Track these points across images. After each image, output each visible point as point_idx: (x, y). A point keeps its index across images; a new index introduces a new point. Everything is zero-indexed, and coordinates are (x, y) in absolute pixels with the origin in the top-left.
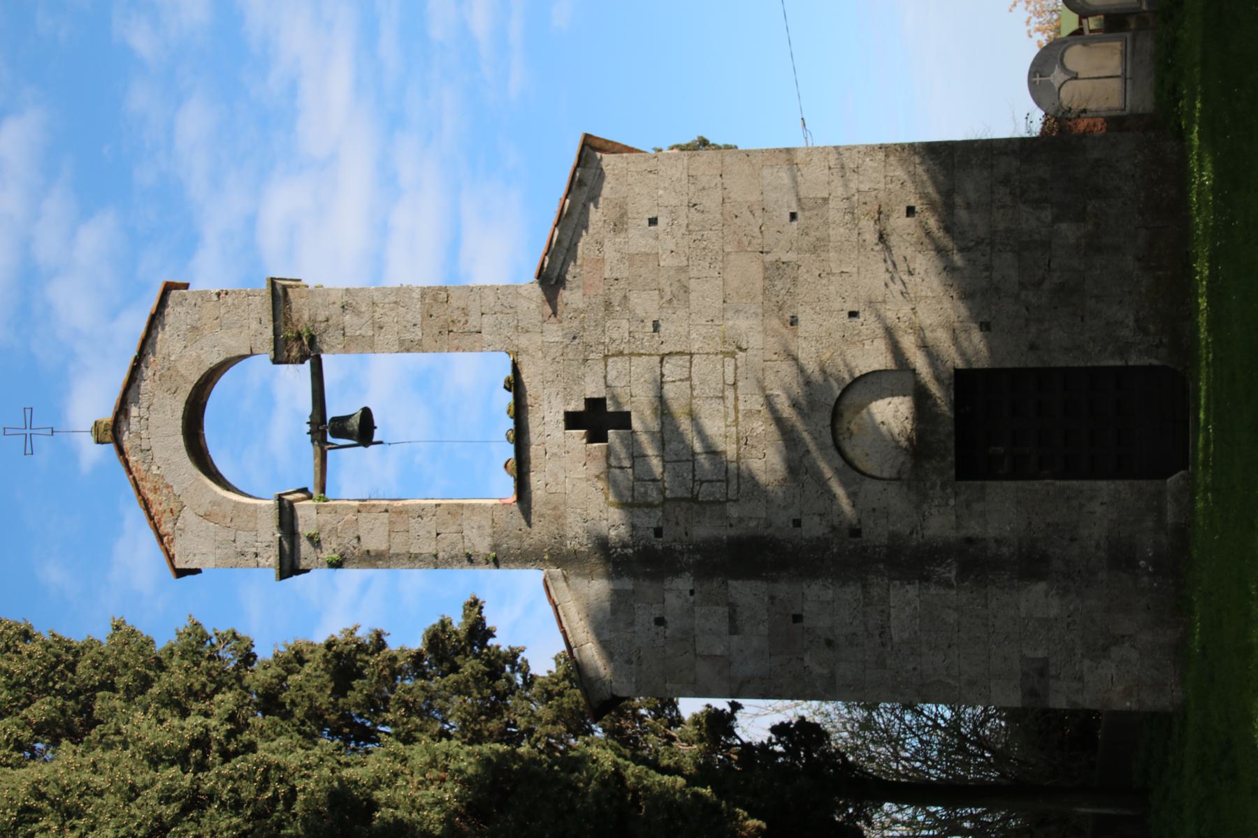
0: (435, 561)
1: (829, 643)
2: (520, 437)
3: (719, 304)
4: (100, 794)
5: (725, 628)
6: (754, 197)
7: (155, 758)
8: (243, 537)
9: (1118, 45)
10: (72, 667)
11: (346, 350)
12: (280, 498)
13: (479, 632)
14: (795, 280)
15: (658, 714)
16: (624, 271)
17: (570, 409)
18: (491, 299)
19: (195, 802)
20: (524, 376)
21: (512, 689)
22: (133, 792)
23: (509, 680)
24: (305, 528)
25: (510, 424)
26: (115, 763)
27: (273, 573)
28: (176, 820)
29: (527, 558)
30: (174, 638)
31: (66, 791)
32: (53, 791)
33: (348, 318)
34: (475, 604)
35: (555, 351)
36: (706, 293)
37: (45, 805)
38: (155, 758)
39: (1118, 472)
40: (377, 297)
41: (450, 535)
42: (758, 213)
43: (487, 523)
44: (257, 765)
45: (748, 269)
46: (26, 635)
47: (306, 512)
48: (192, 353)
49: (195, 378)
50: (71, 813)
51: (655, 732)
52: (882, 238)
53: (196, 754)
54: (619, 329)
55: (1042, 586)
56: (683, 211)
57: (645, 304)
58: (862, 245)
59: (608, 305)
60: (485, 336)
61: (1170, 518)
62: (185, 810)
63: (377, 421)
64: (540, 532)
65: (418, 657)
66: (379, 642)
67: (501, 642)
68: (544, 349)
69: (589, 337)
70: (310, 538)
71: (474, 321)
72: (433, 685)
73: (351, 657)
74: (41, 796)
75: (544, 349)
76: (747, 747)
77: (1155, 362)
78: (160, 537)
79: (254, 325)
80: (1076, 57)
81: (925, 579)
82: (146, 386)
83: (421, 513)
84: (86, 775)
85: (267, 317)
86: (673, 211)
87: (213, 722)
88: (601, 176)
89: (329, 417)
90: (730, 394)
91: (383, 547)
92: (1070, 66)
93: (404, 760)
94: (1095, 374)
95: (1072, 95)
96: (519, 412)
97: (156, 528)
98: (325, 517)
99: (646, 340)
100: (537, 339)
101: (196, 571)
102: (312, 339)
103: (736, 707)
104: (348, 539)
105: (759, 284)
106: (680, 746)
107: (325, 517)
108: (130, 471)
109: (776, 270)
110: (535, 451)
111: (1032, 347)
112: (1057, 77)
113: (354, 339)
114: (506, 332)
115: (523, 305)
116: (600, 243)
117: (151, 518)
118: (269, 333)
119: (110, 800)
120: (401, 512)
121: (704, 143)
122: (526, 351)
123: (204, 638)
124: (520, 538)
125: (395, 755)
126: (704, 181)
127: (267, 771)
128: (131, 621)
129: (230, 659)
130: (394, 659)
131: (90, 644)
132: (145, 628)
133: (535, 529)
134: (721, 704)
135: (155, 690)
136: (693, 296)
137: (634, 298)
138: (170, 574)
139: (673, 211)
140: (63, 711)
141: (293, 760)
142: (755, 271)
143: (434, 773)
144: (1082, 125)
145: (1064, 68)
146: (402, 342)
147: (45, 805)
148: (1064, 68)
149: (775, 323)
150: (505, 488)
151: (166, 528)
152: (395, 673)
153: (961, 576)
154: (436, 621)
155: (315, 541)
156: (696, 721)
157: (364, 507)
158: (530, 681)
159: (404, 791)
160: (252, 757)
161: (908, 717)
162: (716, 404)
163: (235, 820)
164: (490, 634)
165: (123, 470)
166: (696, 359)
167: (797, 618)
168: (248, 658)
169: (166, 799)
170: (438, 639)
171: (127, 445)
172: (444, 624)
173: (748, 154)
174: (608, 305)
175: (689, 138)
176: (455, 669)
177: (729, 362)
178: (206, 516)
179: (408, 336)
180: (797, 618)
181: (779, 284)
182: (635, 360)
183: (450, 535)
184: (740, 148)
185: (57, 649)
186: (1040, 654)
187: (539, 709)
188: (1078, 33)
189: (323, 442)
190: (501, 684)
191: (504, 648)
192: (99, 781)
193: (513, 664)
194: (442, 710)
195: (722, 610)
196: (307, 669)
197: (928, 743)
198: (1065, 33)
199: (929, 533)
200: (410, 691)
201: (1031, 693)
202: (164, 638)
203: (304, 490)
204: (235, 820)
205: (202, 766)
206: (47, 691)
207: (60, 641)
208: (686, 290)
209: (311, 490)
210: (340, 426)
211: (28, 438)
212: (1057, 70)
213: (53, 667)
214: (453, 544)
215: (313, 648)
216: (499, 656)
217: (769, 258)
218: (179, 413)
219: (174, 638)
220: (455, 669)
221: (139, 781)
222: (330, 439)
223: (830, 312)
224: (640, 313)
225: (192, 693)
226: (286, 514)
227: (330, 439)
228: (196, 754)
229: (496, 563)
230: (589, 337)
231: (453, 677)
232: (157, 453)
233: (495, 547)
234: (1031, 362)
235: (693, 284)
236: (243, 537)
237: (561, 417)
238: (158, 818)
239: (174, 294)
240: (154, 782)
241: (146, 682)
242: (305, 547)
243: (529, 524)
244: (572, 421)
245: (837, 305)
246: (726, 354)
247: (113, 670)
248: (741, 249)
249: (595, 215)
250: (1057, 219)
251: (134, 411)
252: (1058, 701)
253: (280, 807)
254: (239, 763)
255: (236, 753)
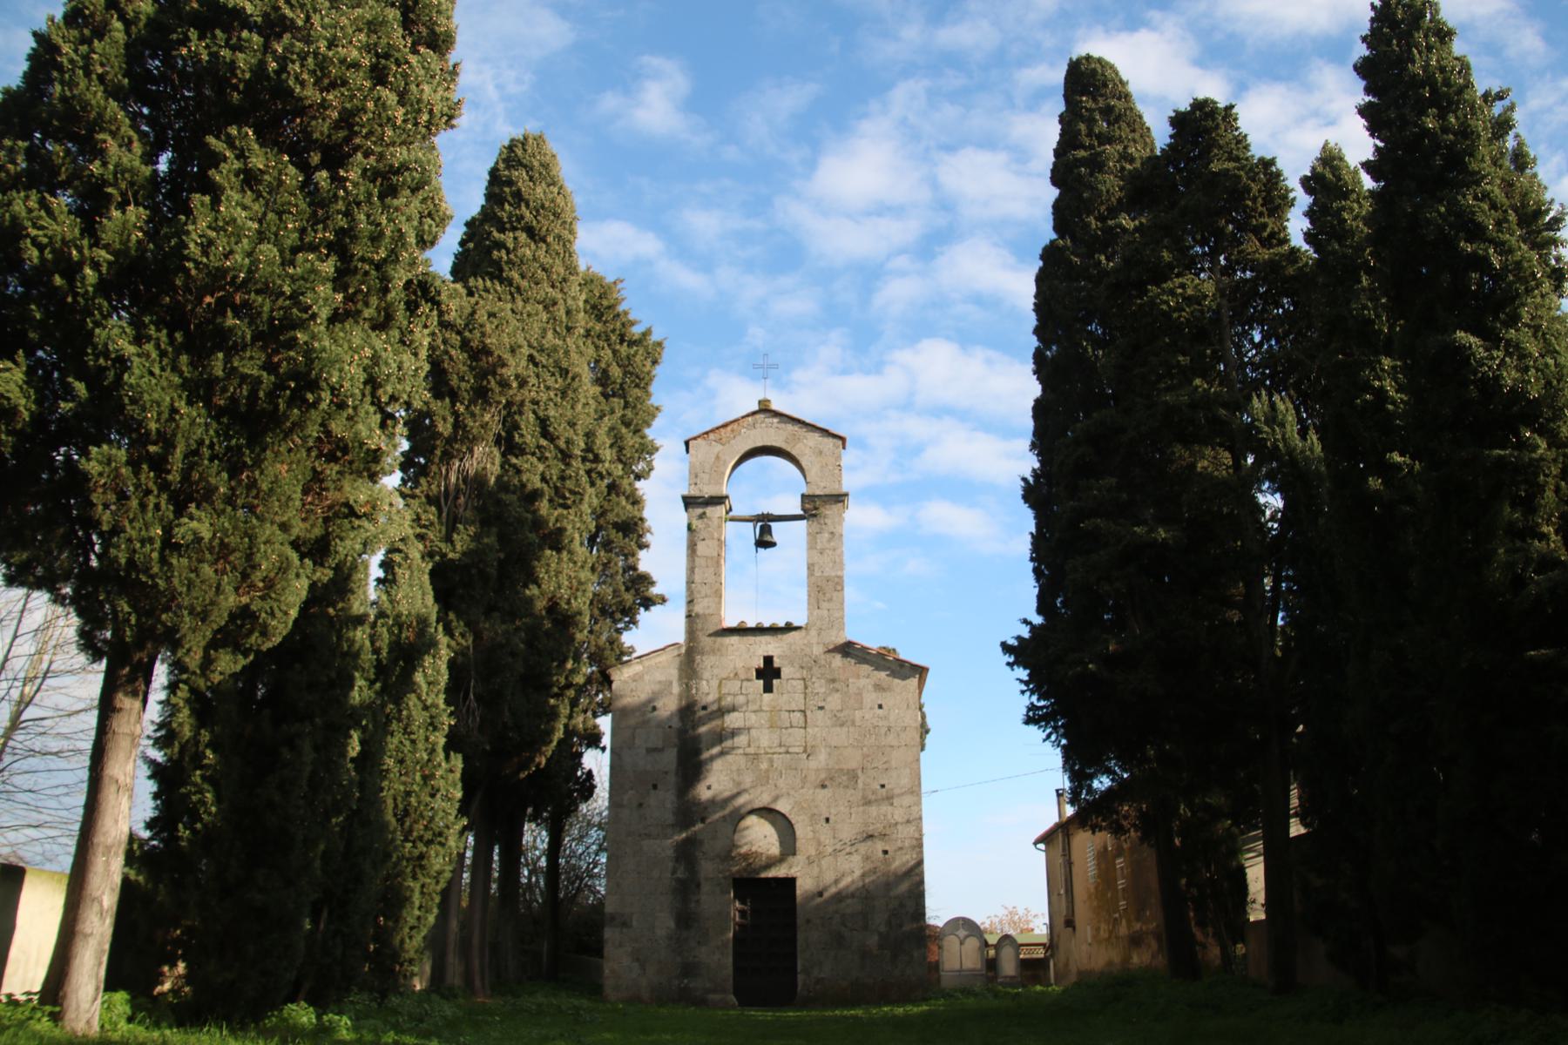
0: (690, 582)
1: (641, 805)
2: (759, 630)
3: (833, 744)
4: (572, 408)
5: (650, 745)
6: (894, 764)
7: (589, 435)
8: (706, 477)
9: (979, 966)
10: (637, 386)
11: (809, 534)
12: (727, 497)
13: (648, 603)
14: (847, 787)
15: (600, 705)
16: (852, 689)
17: (775, 659)
18: (837, 615)
19: (566, 456)
20: (793, 634)
21: (615, 621)
22: (572, 424)
23: (620, 620)
24: (709, 510)
25: (767, 625)
26: (588, 414)
27: (686, 493)
28: (557, 447)
29: (691, 633)
30: (650, 438)
31: (575, 391)
32: (575, 384)
33: (826, 535)
34: (663, 600)
35: (808, 650)
36: (840, 736)
37: (569, 380)
38: (589, 435)
39: (738, 969)
40: (838, 552)
41: (705, 590)
42: (885, 766)
43: (711, 611)
44: (584, 489)
45: (853, 761)
46: (655, 362)
47: (720, 511)
48: (807, 451)
49: (794, 452)
50: (564, 394)
51: (590, 703)
52: (871, 837)
53: (591, 456)
54: (819, 686)
55: (672, 924)
56: (886, 723)
57: (834, 701)
58: (866, 825)
59: (833, 681)
60: (816, 612)
61: (711, 997)
62: (561, 451)
63: (769, 550)
64: (705, 642)
65: (634, 568)
66: (643, 546)
67: (643, 615)
68: (809, 645)
69: (815, 669)
70: (704, 513)
71: (825, 605)
72: (619, 577)
73: (635, 531)
74: (573, 379)
75: (809, 645)
76: (580, 755)
77: (799, 988)
78: (707, 433)
79: (822, 485)
80: (973, 943)
81: (677, 860)
82: (790, 427)
83: (717, 574)
84: (583, 400)
85: (827, 492)
86: (886, 718)
87: (607, 465)
88: (904, 678)
89: (772, 524)
90: (783, 750)
91: (699, 553)
92: (968, 940)
93: (582, 567)
94: (793, 956)
95: (951, 943)
96: (773, 630)
97: (712, 431)
98: (716, 521)
99: (814, 702)
100: (814, 640)
101: (687, 451)
102: (815, 516)
103: (604, 749)
104: (703, 534)
105: (845, 767)
106: (580, 719)
107: (716, 521)
108: (743, 417)
109: (853, 776)
110: (751, 639)
111: (808, 921)
112: (962, 933)
113: (815, 538)
114: (818, 623)
115: (834, 632)
116: (868, 677)
117: (718, 428)
118: (818, 492)
119: (569, 413)
120: (718, 564)
121: (927, 731)
122: (807, 634)
123: (651, 454)
124: (702, 630)
125: (585, 562)
126: (903, 735)
127: (579, 493)
128: (660, 415)
129: (639, 467)
130: (633, 555)
131: (649, 395)
132: (657, 423)
133: (708, 639)
134: (606, 740)
135: (624, 430)
136: (838, 729)
137: (837, 696)
138: (687, 438)
139: (886, 718)
140: (614, 382)
141: (585, 508)
142: (853, 764)
143: (575, 582)
144: (935, 948)
145: (967, 937)
146: (813, 565)
147: (569, 380)
148: (967, 937)
149: (823, 776)
150: (730, 622)
151: (712, 436)
152: (626, 556)
153: (679, 880)
154: (655, 579)
155: (702, 516)
156: (596, 727)
157: (721, 543)
158: (619, 631)
159: (567, 568)
160: (588, 486)
161: (594, 847)
162: (776, 742)
163: (555, 478)
164: (647, 608)
165: (744, 413)
166: (802, 731)
167: (655, 787)
168: (638, 477)
169: (568, 442)
170: (646, 580)
171: (758, 416)
172: (653, 583)
173: (918, 760)
174: (833, 681)
175: (930, 722)
176: (627, 589)
177: (801, 749)
178: (718, 457)
179: (816, 568)
180: (655, 787)
181: (845, 778)
182: (802, 696)
183: (705, 590)
184: (922, 755)
185: (647, 378)
186: (635, 923)
187: (604, 637)
188: (986, 944)
189: (758, 521)
190: (618, 616)
191: (638, 617)
192: (579, 407)
193: (629, 622)
194: (604, 583)
195: (660, 744)
196: (629, 507)
197: (580, 859)
198: (987, 937)
199: (703, 862)
200: (616, 564)
201: (613, 918)
202: (650, 433)
203: (731, 509)
204: (555, 478)
205: (584, 459)
206: (625, 373)
207: (651, 380)
208: (842, 725)
209: (731, 514)
210: (766, 530)
211: (762, 367)
212: (966, 933)
213: (637, 377)
214: (699, 592)
215: (641, 510)
216: (635, 614)
217: (859, 772)
218: (774, 444)
219: (650, 438)
220: (627, 589)
221: (578, 427)
222: (759, 524)
223: (829, 807)
224: (829, 699)
225: (621, 449)
226: (719, 500)
227: (759, 524)
228: (591, 456)
229: (689, 616)
230: (815, 669)
231: (623, 588)
232: (753, 432)
233: (698, 615)
234: (800, 921)
235: (845, 729)
236: (706, 477)
237: (770, 654)
238: (558, 438)
239: (840, 442)
240: (577, 435)
241: (627, 424)
242: (699, 511)
243: (710, 635)
244: (768, 660)
245: (833, 811)
246: (805, 747)
247: (635, 407)
248: (865, 756)
249: (883, 674)
250: (880, 934)
251: (776, 420)
252: (608, 933)
253: (561, 501)
254: (584, 479)
255: (590, 477)
